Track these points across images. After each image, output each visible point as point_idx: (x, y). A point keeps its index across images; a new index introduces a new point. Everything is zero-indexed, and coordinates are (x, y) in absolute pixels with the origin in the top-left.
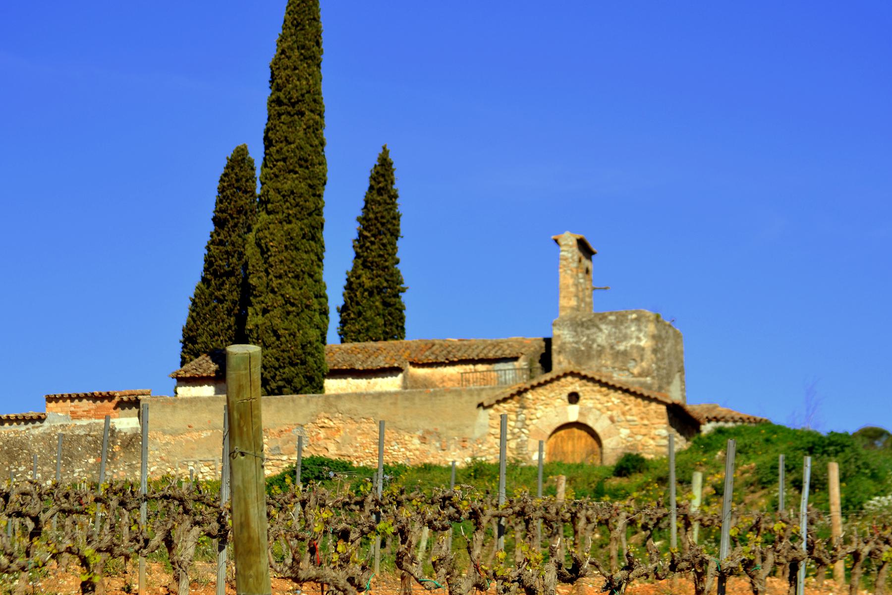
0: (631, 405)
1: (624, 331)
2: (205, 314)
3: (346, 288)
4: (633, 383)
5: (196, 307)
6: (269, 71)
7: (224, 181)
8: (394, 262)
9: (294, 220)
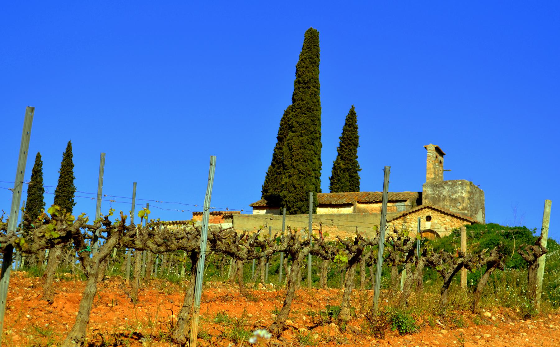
0: (455, 223)
1: (455, 189)
2: (272, 180)
3: (333, 169)
4: (459, 213)
5: (269, 176)
6: (296, 68)
7: (283, 121)
8: (355, 157)
9: (304, 135)
